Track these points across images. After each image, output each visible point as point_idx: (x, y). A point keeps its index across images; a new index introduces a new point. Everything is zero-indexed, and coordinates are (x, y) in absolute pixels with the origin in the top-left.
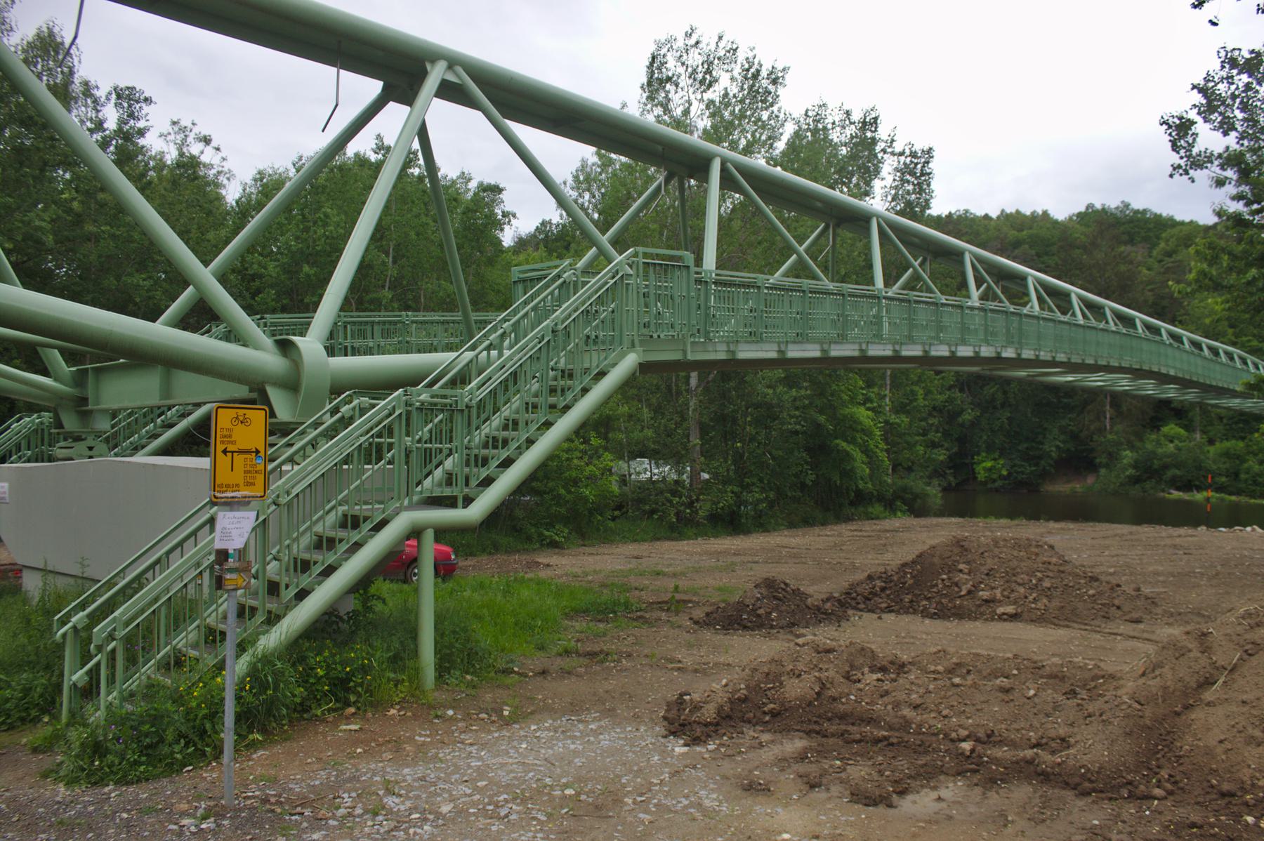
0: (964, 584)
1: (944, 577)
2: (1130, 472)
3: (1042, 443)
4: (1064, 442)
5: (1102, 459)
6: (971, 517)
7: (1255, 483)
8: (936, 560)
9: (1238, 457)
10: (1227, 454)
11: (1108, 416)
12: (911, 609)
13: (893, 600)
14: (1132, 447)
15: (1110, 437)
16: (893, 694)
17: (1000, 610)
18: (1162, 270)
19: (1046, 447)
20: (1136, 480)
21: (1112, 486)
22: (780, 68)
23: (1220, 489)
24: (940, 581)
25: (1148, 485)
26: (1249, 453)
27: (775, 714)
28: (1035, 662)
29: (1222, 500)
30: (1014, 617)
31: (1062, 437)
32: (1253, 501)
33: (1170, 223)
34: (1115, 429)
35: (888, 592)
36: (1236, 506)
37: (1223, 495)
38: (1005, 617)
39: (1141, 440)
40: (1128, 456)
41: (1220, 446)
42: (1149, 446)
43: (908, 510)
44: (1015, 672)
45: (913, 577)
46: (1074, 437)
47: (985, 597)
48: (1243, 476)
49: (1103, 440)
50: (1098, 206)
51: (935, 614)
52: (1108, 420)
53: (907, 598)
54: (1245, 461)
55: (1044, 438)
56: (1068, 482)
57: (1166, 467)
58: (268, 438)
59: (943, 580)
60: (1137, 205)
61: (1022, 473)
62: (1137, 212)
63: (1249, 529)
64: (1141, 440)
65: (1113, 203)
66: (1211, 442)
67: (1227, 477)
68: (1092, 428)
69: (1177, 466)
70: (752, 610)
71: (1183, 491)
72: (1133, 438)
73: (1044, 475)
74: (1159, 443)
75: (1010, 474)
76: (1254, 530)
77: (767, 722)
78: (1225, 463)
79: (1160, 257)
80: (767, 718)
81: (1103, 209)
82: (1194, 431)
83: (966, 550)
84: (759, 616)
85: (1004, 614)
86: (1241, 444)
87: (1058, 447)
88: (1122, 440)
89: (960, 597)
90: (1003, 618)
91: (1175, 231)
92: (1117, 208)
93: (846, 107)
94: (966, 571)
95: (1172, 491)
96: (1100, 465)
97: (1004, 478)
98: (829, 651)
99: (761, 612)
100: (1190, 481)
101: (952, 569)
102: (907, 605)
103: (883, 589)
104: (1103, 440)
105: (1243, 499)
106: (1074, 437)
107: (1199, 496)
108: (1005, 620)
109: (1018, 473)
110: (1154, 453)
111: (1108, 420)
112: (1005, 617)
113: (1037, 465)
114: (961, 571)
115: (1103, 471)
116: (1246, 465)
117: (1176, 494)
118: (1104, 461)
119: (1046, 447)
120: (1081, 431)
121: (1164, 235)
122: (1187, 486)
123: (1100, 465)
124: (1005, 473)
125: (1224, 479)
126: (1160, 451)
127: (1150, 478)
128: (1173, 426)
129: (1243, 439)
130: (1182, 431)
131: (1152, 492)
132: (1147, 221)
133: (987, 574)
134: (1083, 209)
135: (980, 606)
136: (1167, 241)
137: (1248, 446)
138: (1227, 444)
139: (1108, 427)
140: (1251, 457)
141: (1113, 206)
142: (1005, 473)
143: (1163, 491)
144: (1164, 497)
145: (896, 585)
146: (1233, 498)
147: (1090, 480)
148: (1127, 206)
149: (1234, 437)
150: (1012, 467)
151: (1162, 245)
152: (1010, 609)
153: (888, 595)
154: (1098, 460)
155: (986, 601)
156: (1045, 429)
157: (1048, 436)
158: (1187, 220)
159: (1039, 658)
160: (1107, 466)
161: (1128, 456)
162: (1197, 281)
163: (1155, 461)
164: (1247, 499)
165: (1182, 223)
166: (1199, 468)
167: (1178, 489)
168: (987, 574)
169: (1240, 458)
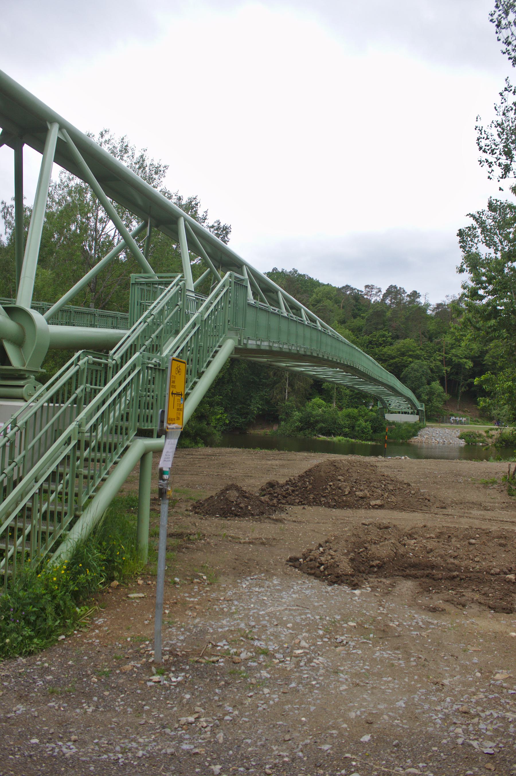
0: (345, 488)
1: (331, 483)
2: (298, 424)
3: (250, 405)
4: (261, 405)
5: (282, 416)
6: (245, 448)
7: (363, 432)
8: (322, 474)
9: (354, 418)
10: (348, 416)
11: (287, 391)
12: (316, 502)
13: (302, 498)
14: (299, 410)
15: (287, 403)
16: (437, 551)
17: (373, 503)
18: (316, 310)
19: (252, 408)
20: (300, 429)
21: (288, 432)
22: (163, 165)
23: (345, 435)
24: (328, 486)
25: (307, 432)
26: (360, 415)
27: (379, 567)
28: (484, 530)
29: (348, 441)
30: (381, 507)
31: (261, 402)
32: (363, 442)
33: (315, 284)
34: (290, 398)
35: (297, 493)
36: (353, 445)
37: (348, 438)
38: (377, 507)
39: (304, 406)
40: (297, 414)
41: (345, 411)
42: (309, 410)
43: (204, 443)
44: (477, 536)
45: (310, 484)
46: (268, 402)
47: (360, 496)
48: (357, 428)
49: (284, 405)
50: (280, 270)
51: (335, 505)
52: (286, 394)
53: (311, 496)
54: (358, 420)
55: (251, 402)
56: (263, 428)
57: (317, 422)
58: (171, 384)
59: (330, 486)
60: (301, 272)
61: (237, 422)
62: (300, 275)
63: (403, 458)
64: (304, 406)
65: (288, 269)
66: (341, 408)
67: (349, 428)
68: (278, 397)
69: (323, 422)
70: (236, 504)
71: (326, 436)
72: (299, 405)
73: (250, 424)
74: (313, 409)
75: (230, 422)
76: (405, 458)
77: (376, 572)
78: (347, 421)
79: (313, 303)
80: (376, 569)
81: (282, 272)
82: (332, 403)
83: (337, 468)
84: (241, 508)
85: (376, 505)
86: (356, 411)
87: (258, 408)
88: (294, 405)
89: (344, 495)
90: (374, 507)
91: (322, 288)
92: (290, 272)
93: (179, 195)
94: (343, 480)
95: (320, 436)
96: (282, 420)
97: (227, 425)
98: (387, 528)
99: (242, 505)
100: (329, 430)
101: (333, 478)
102: (312, 500)
103: (293, 491)
104: (284, 405)
105: (358, 441)
106: (268, 402)
107: (336, 439)
108: (377, 508)
109: (234, 422)
110: (311, 413)
111: (286, 394)
112: (377, 507)
113: (245, 418)
114: (339, 480)
115: (283, 423)
116: (358, 423)
117: (323, 438)
118: (284, 417)
119: (252, 408)
120: (272, 399)
121: (315, 290)
122: (328, 433)
123: (282, 420)
124: (228, 422)
125: (347, 430)
126: (314, 413)
127: (308, 428)
128: (318, 399)
129: (357, 408)
130: (323, 402)
131: (309, 436)
132: (306, 281)
133: (355, 482)
134: (271, 271)
135: (357, 501)
136: (317, 294)
137: (359, 412)
138: (350, 410)
139: (286, 398)
140: (360, 418)
141: (288, 271)
142: (228, 422)
143: (315, 435)
144: (316, 439)
145: (300, 489)
146: (353, 440)
147: (275, 428)
148: (296, 271)
149: (352, 406)
150: (232, 418)
151: (314, 296)
152: (378, 502)
153: (297, 495)
154: (280, 417)
155: (361, 498)
156: (252, 397)
157: (253, 401)
158: (326, 283)
159: (487, 527)
160: (285, 420)
161: (297, 414)
162: (464, 323)
163: (312, 418)
164: (360, 441)
165: (324, 285)
166: (335, 423)
167: (323, 434)
168: (355, 482)
169: (356, 419)
